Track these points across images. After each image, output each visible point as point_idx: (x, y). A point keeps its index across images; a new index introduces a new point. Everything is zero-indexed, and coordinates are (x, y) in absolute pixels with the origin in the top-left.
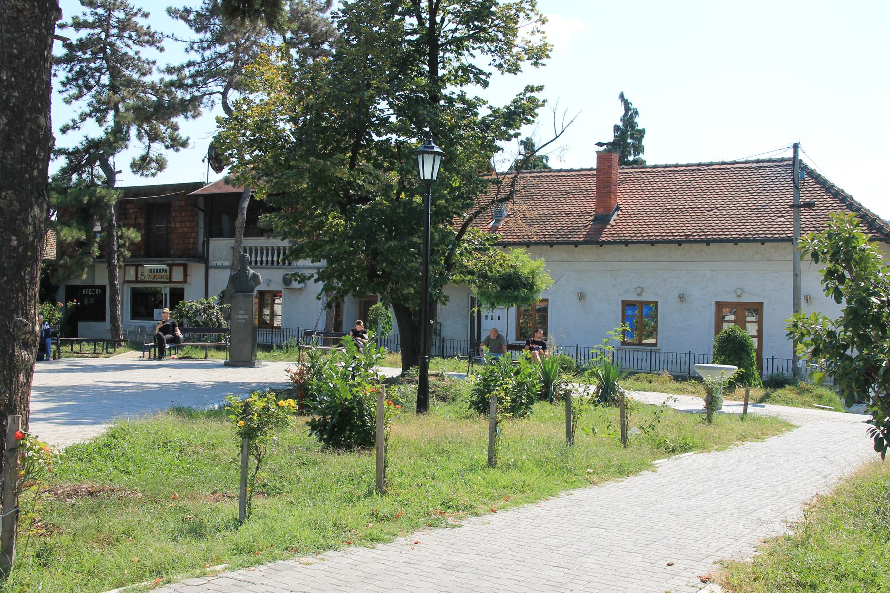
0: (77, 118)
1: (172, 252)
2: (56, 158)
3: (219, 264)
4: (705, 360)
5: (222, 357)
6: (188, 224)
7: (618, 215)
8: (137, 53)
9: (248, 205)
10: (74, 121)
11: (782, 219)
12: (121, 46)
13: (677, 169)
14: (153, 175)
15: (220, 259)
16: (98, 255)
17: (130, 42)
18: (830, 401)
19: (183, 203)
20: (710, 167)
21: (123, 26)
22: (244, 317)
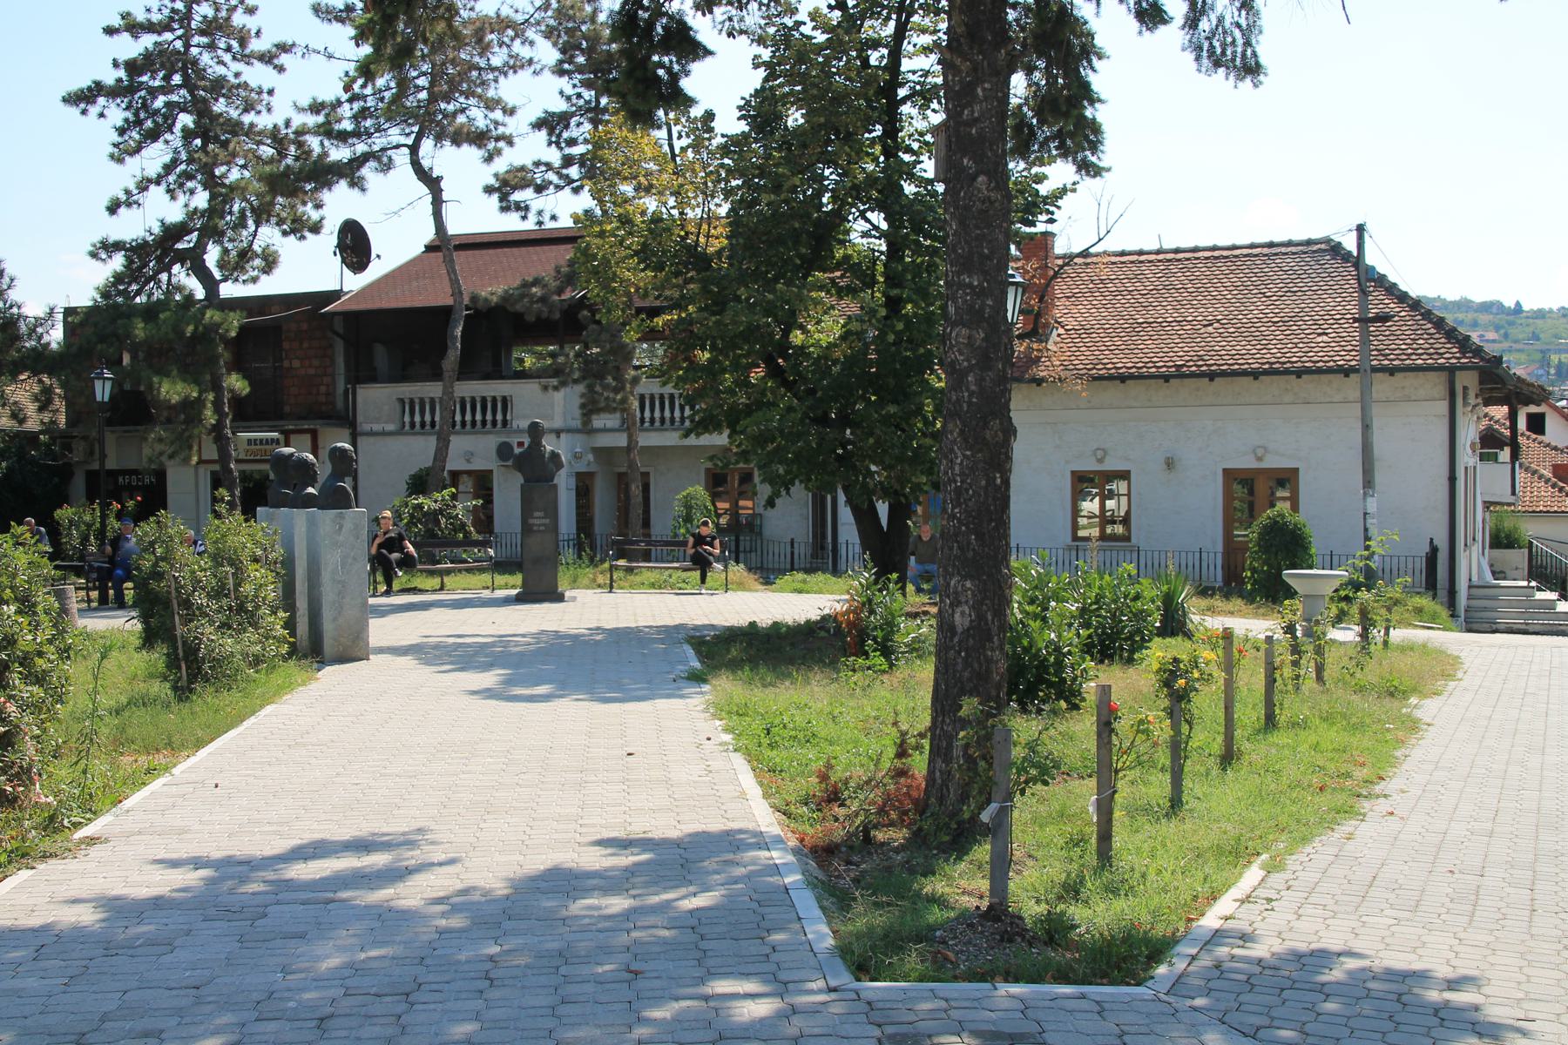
0: (132, 187)
1: (287, 409)
2: (110, 257)
3: (377, 427)
4: (1328, 564)
5: (511, 584)
6: (316, 362)
7: (1059, 335)
8: (237, 75)
9: (462, 332)
10: (128, 192)
11: (1325, 338)
12: (211, 63)
13: (1142, 258)
14: (254, 280)
15: (377, 421)
16: (213, 422)
17: (227, 58)
18: (1434, 617)
19: (305, 326)
20: (1196, 255)
21: (213, 28)
22: (544, 521)
